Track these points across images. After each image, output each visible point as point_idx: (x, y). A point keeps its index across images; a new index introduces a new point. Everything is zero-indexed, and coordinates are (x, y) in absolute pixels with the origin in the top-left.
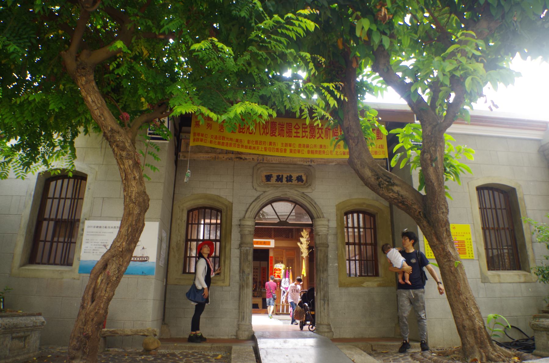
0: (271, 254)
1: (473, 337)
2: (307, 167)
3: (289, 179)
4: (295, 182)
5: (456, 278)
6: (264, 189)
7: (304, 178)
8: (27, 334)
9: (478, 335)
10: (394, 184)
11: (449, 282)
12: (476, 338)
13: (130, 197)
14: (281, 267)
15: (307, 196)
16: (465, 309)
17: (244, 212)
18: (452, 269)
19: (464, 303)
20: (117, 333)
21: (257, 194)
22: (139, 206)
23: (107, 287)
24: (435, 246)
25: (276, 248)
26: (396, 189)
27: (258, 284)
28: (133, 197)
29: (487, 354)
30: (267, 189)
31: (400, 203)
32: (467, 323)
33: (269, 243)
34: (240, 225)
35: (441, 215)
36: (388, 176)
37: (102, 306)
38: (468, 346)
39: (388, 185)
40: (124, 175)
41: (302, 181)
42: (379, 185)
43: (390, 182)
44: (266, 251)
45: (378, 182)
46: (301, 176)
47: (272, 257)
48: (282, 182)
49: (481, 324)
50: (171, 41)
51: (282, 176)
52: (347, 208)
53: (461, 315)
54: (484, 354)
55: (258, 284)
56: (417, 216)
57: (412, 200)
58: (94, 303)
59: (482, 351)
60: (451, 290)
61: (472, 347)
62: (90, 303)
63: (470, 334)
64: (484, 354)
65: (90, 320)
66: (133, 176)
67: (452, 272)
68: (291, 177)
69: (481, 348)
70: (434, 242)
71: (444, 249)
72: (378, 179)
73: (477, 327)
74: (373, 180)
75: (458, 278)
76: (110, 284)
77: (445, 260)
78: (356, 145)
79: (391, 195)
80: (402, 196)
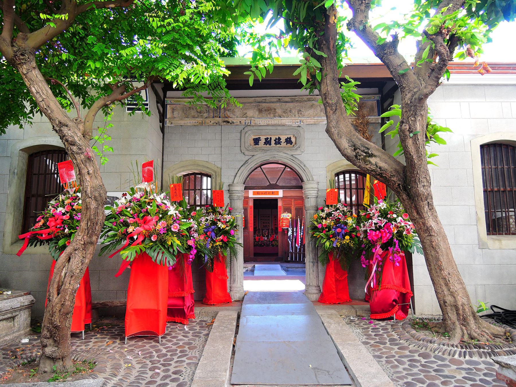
0: (280, 204)
1: (455, 313)
2: (296, 128)
3: (278, 141)
4: (283, 144)
5: (438, 253)
6: (252, 153)
7: (293, 140)
8: (14, 314)
9: (461, 312)
10: (372, 155)
11: (430, 257)
12: (458, 314)
13: (86, 192)
14: (288, 216)
15: (296, 158)
16: (447, 285)
17: (233, 177)
18: (433, 243)
19: (445, 279)
20: (108, 305)
21: (247, 158)
22: (96, 200)
23: (70, 281)
24: (415, 220)
25: (284, 197)
26: (373, 160)
27: (270, 231)
28: (89, 191)
29: (469, 332)
30: (255, 153)
31: (379, 175)
32: (449, 299)
33: (277, 193)
34: (229, 190)
35: (422, 189)
36: (366, 146)
37: (67, 298)
38: (449, 322)
39: (365, 156)
40: (78, 170)
41: (291, 143)
42: (356, 156)
43: (368, 153)
44: (276, 200)
45: (354, 154)
46: (290, 138)
47: (280, 207)
48: (270, 144)
49: (465, 301)
50: (43, 65)
51: (271, 138)
52: (338, 169)
53: (443, 291)
54: (465, 332)
55: (270, 231)
56: (397, 188)
57: (391, 172)
58: (60, 295)
59: (464, 328)
60: (432, 264)
61: (454, 323)
62: (56, 296)
63: (452, 310)
64: (465, 332)
65: (57, 311)
66: (86, 171)
67: (433, 247)
68: (279, 139)
69: (463, 324)
70: (414, 216)
71: (424, 224)
72: (355, 150)
73: (460, 303)
74: (350, 151)
75: (440, 253)
76: (74, 277)
77: (426, 235)
78: (334, 113)
79: (368, 167)
80: (380, 168)
